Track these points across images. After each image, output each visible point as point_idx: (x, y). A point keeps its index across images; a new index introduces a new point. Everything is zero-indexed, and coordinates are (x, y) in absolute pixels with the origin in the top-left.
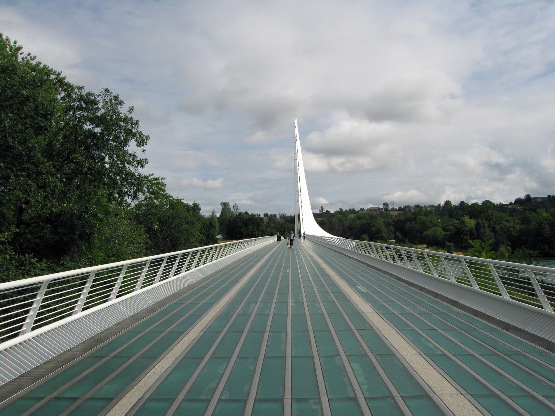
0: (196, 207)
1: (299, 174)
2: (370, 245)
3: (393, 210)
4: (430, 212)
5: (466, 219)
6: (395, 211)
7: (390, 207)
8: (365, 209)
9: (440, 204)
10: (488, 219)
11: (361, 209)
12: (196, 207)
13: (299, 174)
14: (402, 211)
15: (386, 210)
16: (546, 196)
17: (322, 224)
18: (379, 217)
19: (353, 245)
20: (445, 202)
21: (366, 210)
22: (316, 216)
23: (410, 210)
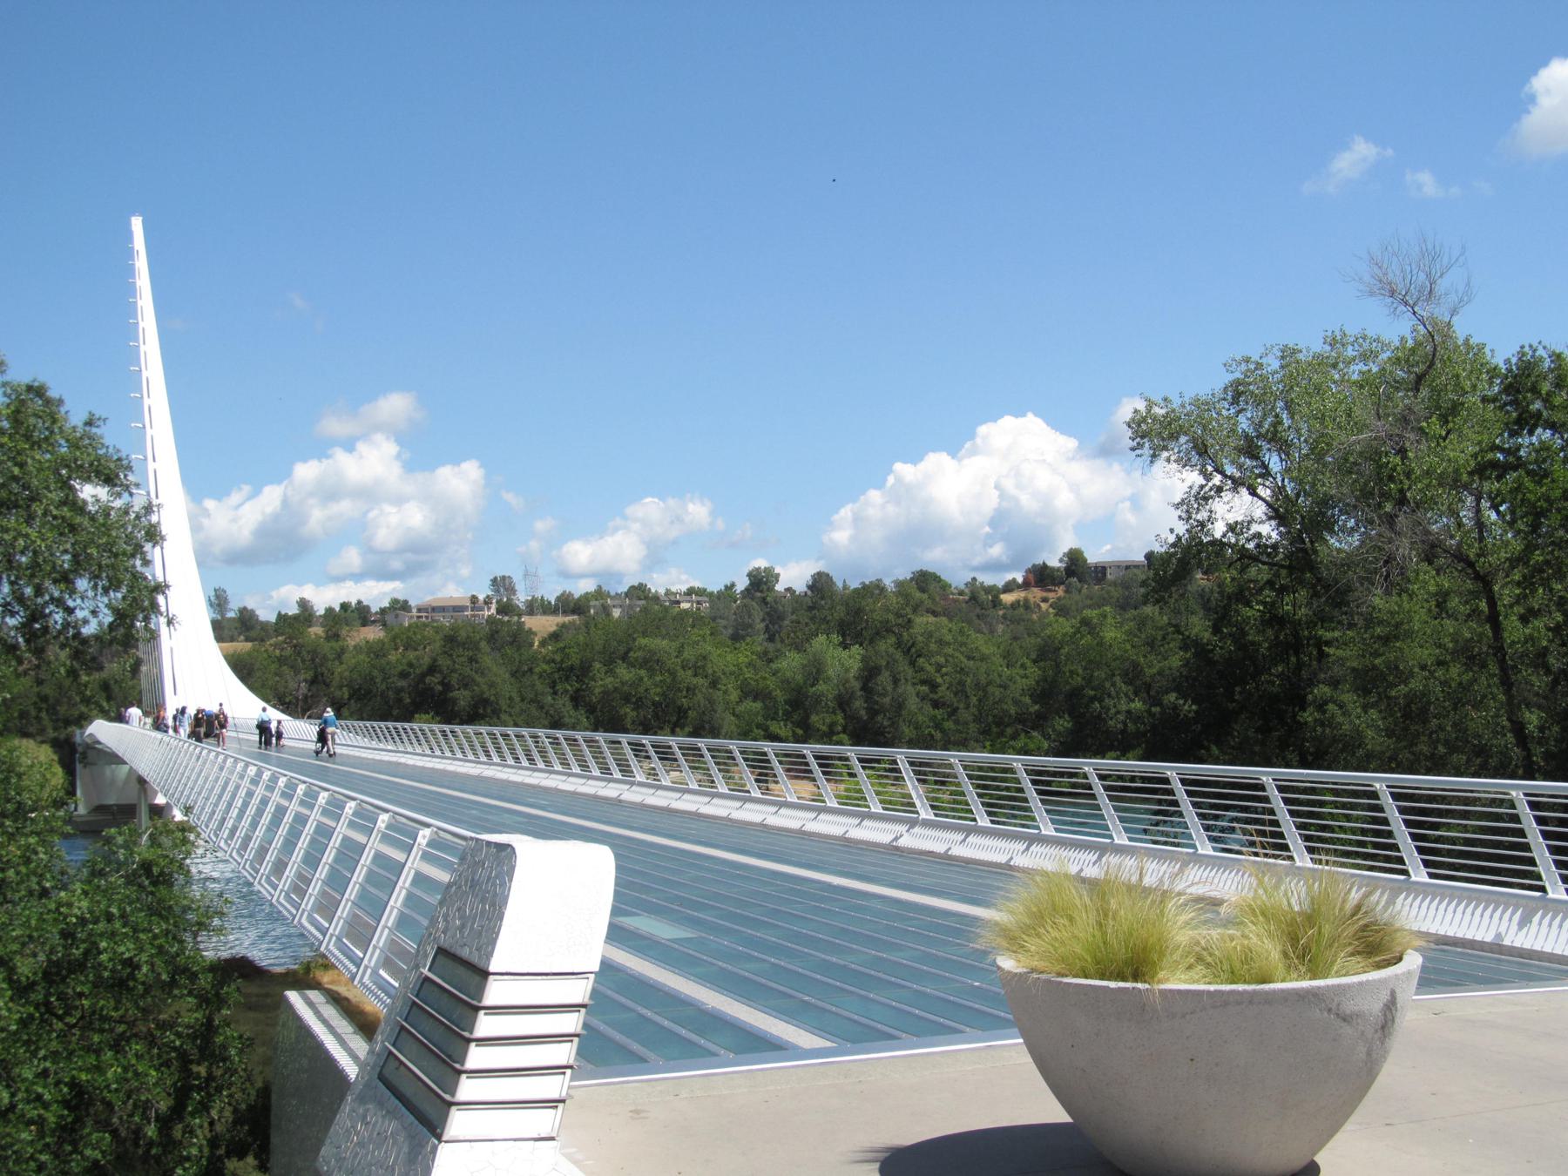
0: (761, 582)
1: (154, 460)
2: (444, 731)
3: (537, 607)
4: (696, 619)
5: (824, 645)
6: (545, 613)
7: (521, 598)
8: (413, 603)
9: (733, 585)
10: (911, 652)
11: (395, 601)
12: (761, 582)
13: (154, 460)
14: (574, 612)
15: (505, 609)
16: (1139, 557)
17: (244, 669)
18: (483, 644)
19: (389, 1126)
20: (750, 575)
21: (419, 610)
22: (221, 630)
23: (606, 610)
